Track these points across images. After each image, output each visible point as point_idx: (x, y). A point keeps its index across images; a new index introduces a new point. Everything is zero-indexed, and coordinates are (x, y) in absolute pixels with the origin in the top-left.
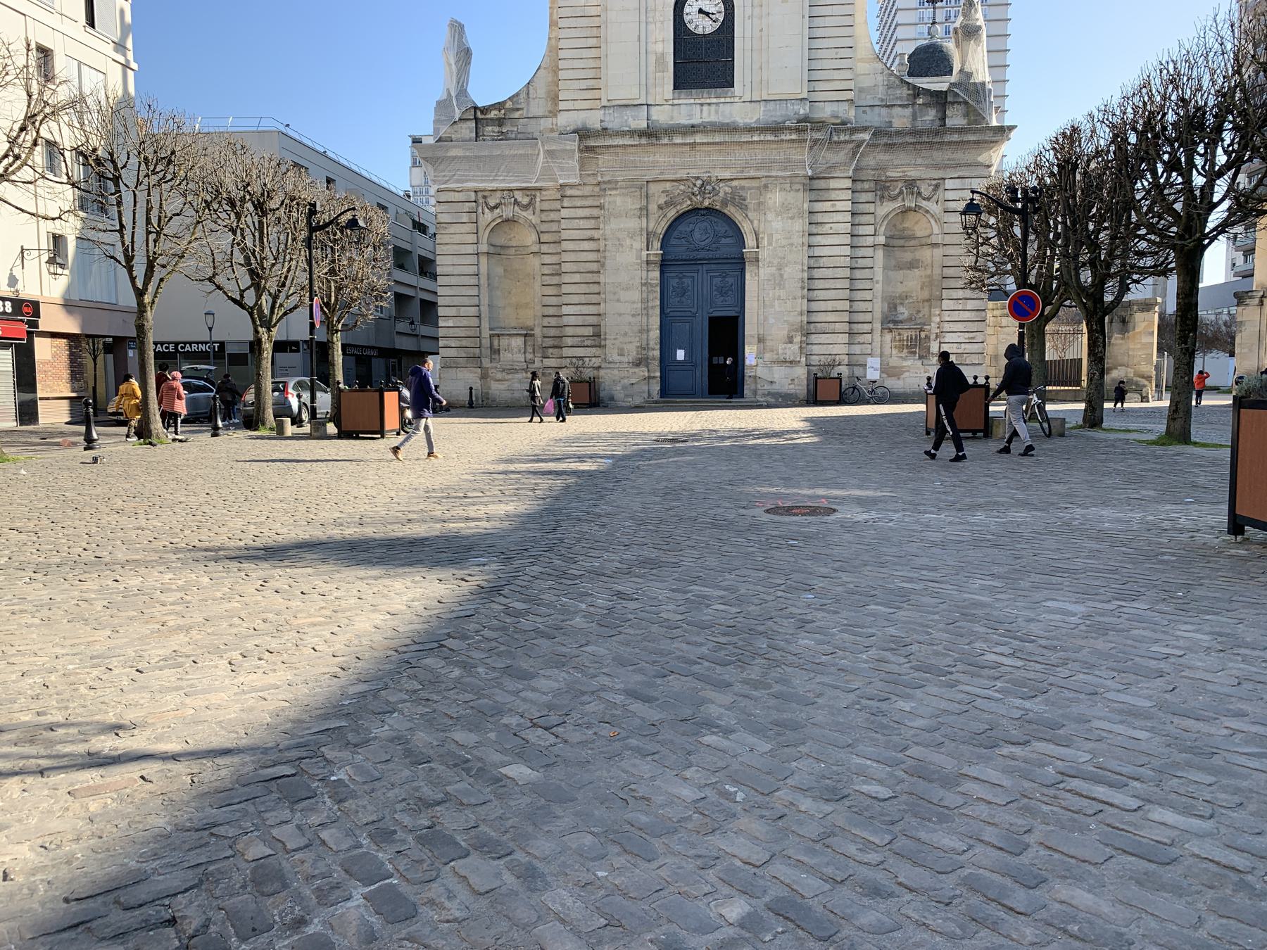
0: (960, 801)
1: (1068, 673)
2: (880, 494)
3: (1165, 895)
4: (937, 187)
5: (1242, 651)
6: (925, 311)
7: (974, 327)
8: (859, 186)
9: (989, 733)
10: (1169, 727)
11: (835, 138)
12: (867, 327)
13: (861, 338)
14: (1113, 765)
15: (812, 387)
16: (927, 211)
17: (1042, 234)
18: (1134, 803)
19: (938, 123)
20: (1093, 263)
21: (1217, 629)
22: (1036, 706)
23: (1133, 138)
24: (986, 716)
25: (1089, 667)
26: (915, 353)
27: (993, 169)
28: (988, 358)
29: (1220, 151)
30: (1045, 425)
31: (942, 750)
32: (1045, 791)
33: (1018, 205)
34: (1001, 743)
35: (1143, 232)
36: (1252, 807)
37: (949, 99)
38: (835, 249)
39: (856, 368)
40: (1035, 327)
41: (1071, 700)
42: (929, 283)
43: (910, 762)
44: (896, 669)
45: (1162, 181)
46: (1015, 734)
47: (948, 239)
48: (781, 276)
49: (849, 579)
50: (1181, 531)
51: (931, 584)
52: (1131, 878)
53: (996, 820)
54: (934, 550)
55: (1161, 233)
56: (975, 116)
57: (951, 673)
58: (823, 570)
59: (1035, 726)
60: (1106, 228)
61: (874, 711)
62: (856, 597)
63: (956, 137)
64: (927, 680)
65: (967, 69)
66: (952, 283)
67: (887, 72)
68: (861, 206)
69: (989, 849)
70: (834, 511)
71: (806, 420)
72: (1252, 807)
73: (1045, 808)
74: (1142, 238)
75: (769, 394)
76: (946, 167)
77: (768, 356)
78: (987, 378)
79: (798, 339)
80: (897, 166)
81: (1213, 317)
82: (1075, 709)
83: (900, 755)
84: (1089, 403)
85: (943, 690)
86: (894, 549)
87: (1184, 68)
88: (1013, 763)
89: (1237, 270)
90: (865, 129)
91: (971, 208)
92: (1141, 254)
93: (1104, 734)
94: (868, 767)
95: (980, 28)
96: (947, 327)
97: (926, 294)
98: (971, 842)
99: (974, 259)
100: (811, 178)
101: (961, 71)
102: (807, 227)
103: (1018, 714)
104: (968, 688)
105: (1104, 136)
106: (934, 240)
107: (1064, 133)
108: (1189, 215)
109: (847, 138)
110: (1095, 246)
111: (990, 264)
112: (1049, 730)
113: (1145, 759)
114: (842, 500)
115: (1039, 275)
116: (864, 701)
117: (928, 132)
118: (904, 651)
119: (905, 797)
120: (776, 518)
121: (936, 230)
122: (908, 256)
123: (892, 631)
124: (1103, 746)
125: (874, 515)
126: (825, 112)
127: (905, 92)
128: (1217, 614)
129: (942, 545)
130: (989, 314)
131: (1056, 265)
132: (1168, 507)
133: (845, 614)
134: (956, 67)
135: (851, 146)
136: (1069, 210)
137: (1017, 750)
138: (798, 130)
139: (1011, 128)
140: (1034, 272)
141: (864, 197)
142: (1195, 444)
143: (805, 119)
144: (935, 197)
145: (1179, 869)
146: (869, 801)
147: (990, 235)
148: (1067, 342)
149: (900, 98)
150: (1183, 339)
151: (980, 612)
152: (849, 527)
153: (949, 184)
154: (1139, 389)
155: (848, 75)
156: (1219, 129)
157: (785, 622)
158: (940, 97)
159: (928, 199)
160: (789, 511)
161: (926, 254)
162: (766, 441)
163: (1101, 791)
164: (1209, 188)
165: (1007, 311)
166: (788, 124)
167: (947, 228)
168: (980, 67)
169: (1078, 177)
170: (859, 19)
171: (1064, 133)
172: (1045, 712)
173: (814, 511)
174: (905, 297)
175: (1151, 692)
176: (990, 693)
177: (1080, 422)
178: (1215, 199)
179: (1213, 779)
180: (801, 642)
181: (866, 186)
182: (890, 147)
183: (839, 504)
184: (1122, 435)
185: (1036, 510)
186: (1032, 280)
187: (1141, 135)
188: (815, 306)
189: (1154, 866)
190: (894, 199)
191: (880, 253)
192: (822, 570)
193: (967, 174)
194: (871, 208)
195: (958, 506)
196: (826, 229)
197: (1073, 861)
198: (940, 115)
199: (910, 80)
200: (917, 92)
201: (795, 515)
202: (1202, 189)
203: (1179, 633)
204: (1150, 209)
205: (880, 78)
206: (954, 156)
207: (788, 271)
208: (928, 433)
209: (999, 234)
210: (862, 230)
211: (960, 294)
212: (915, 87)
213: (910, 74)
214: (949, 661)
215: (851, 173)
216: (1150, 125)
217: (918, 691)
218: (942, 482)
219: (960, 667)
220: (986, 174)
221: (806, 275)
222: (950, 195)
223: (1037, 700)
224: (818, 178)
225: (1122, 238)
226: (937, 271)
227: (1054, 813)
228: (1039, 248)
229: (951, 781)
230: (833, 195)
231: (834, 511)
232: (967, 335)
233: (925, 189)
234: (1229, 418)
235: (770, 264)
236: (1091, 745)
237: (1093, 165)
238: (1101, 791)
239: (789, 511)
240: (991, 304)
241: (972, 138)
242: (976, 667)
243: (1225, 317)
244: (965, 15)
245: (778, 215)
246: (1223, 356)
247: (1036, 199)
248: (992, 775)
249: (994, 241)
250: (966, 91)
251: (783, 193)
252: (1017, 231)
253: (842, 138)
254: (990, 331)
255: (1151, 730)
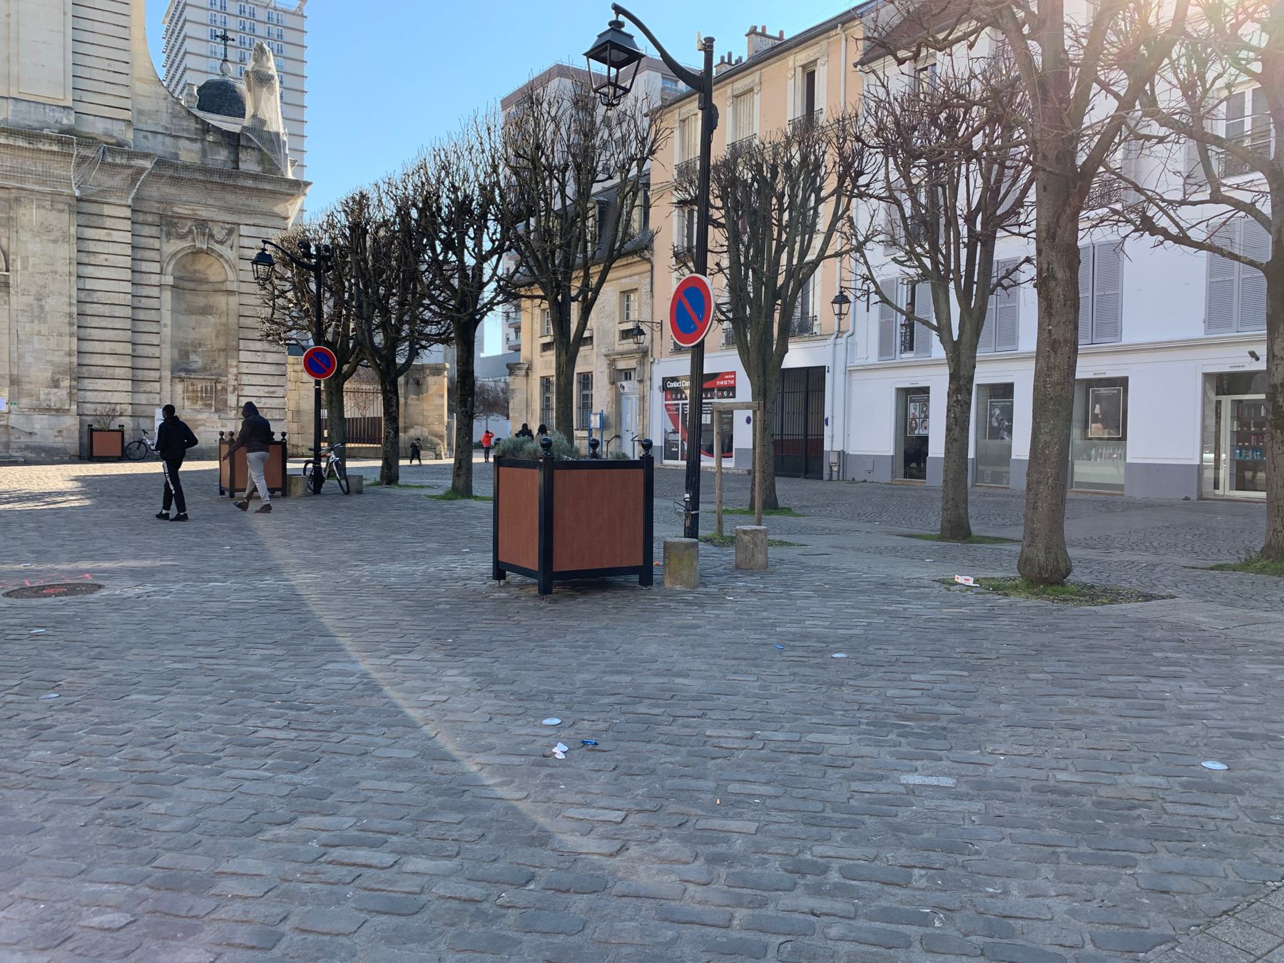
0: (212, 904)
1: (341, 736)
2: (158, 563)
3: (411, 946)
4: (230, 232)
5: (496, 687)
6: (221, 360)
7: (274, 381)
8: (141, 217)
9: (254, 818)
10: (430, 774)
11: (110, 160)
12: (155, 375)
13: (148, 387)
14: (377, 824)
15: (86, 440)
16: (221, 256)
17: (337, 293)
18: (389, 859)
19: (230, 165)
20: (384, 326)
21: (477, 670)
22: (307, 779)
23: (414, 213)
24: (252, 800)
25: (362, 726)
26: (211, 405)
27: (290, 222)
28: (290, 414)
29: (485, 237)
30: (344, 482)
31: (200, 850)
32: (306, 868)
33: (308, 262)
34: (266, 827)
35: (426, 302)
36: (491, 836)
37: (243, 142)
38: (111, 283)
39: (141, 420)
40: (333, 384)
41: (341, 765)
42: (224, 330)
43: (159, 873)
44: (153, 765)
45: (441, 258)
46: (282, 812)
47: (244, 287)
48: (41, 307)
49: (107, 668)
50: (456, 580)
51: (207, 661)
52: (382, 939)
53: (251, 916)
54: (214, 622)
55: (440, 305)
56: (271, 168)
57: (219, 759)
58: (77, 661)
59: (303, 800)
60: (394, 295)
61: (119, 823)
62: (114, 687)
63: (250, 183)
64: (190, 772)
65: (260, 115)
66: (250, 334)
67: (170, 98)
68: (144, 240)
69: (240, 951)
70: (100, 587)
71: (77, 479)
72: (491, 836)
73: (304, 887)
74: (427, 308)
75: (27, 447)
76: (240, 212)
77: (25, 402)
78: (284, 434)
79: (66, 383)
80: (185, 203)
81: (492, 384)
82: (344, 775)
83: (147, 869)
84: (386, 460)
85: (207, 780)
86: (169, 626)
87: (453, 158)
88: (275, 846)
89: (511, 344)
90: (146, 156)
91: (263, 258)
92: (427, 322)
93: (370, 794)
94: (104, 892)
95: (272, 77)
96: (245, 380)
97: (221, 343)
98: (218, 949)
99: (270, 310)
100: (79, 200)
101: (254, 116)
102: (74, 255)
103: (285, 790)
104: (235, 773)
105: (390, 210)
106: (230, 286)
107: (353, 198)
108: (463, 293)
109: (124, 161)
110: (386, 311)
111: (288, 318)
112: (316, 801)
113: (404, 811)
114: (112, 574)
115: (336, 334)
116: (107, 813)
117: (220, 173)
118: (166, 743)
119: (147, 917)
120: (19, 602)
121: (231, 276)
122: (200, 301)
123: (155, 721)
124: (368, 806)
125: (149, 587)
126: (97, 128)
127: (193, 125)
128: (478, 655)
129: (224, 616)
130: (290, 369)
131: (352, 326)
132: (448, 558)
133: (97, 710)
134: (249, 110)
135: (130, 171)
136: (362, 273)
137: (281, 831)
138: (59, 141)
139: (307, 184)
140: (331, 330)
141: (147, 231)
142: (476, 498)
143: (70, 131)
144: (229, 242)
145: (425, 916)
146: (99, 935)
147: (286, 288)
148: (362, 401)
149: (188, 130)
150: (463, 402)
151: (257, 685)
152: (115, 605)
153: (244, 230)
154: (433, 448)
155: (124, 92)
156: (484, 217)
157: (13, 734)
158: (226, 139)
159: (221, 243)
160: (38, 592)
161: (221, 301)
162: (18, 506)
163: (362, 855)
164: (478, 269)
165: (302, 367)
166: (46, 131)
167: (243, 276)
168: (274, 116)
169: (369, 243)
170: (136, 33)
171: (353, 198)
172: (315, 782)
173: (72, 590)
174: (197, 345)
175: (416, 742)
176: (260, 773)
177: (378, 479)
178: (485, 279)
179: (460, 817)
180: (33, 755)
181: (150, 218)
182: (176, 181)
183: (107, 578)
184: (415, 491)
185: (329, 569)
186: (329, 337)
187: (420, 211)
188: (88, 346)
189: (403, 919)
190: (182, 237)
191: (167, 295)
192: (74, 660)
193: (263, 223)
194: (156, 244)
195: (247, 571)
196: (100, 259)
197: (327, 938)
198: (232, 157)
199: (201, 114)
200: (206, 128)
201: (46, 596)
202: (473, 268)
203: (445, 679)
204: (432, 282)
205: (163, 104)
206: (248, 202)
207: (50, 303)
208: (222, 493)
209: (295, 288)
210: (145, 266)
211: (258, 346)
212: (203, 122)
213: (200, 108)
214: (218, 745)
215: (130, 202)
216: (429, 203)
217: (177, 788)
218: (232, 546)
219: (229, 750)
220: (283, 226)
221: (74, 310)
222: (246, 242)
223: (307, 772)
224: (88, 201)
225: (410, 305)
226: (233, 320)
227: (313, 891)
228: (335, 306)
229: (201, 885)
230: (109, 223)
231: (100, 587)
232: (267, 389)
233: (219, 232)
234: (491, 473)
235: (25, 292)
236: (357, 808)
237: (382, 233)
238: (362, 855)
239: (38, 592)
240: (291, 359)
241: (267, 187)
242: (245, 745)
243: (502, 385)
244: (256, 60)
245: (35, 236)
246: (502, 419)
247: (329, 258)
248: (251, 864)
249: (290, 295)
250: (260, 137)
251: (42, 211)
252: (313, 286)
253: (118, 161)
254: (290, 386)
255: (413, 780)
